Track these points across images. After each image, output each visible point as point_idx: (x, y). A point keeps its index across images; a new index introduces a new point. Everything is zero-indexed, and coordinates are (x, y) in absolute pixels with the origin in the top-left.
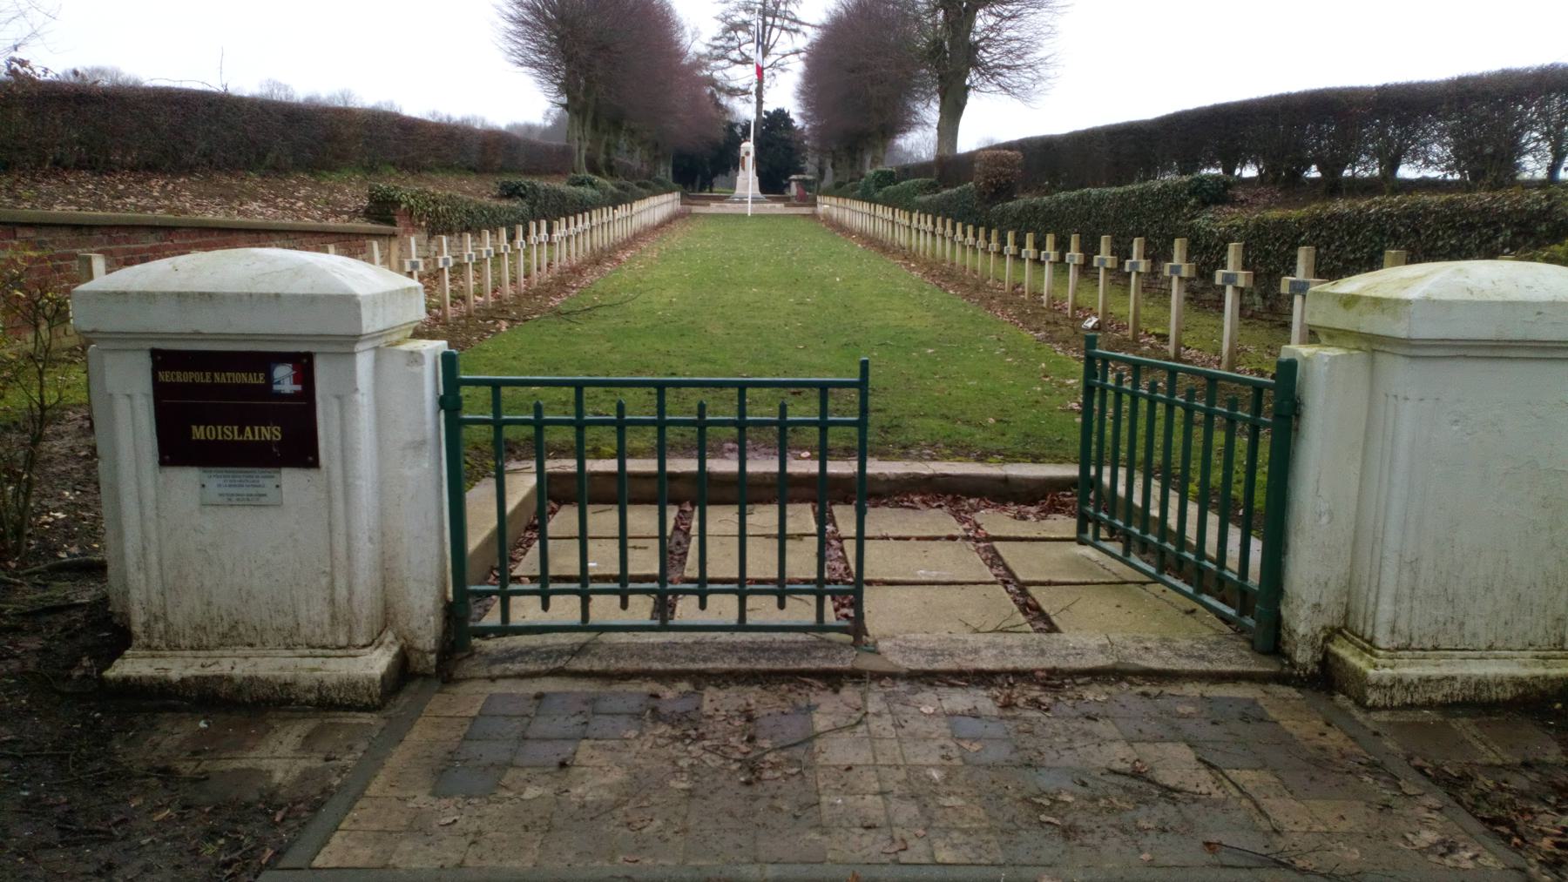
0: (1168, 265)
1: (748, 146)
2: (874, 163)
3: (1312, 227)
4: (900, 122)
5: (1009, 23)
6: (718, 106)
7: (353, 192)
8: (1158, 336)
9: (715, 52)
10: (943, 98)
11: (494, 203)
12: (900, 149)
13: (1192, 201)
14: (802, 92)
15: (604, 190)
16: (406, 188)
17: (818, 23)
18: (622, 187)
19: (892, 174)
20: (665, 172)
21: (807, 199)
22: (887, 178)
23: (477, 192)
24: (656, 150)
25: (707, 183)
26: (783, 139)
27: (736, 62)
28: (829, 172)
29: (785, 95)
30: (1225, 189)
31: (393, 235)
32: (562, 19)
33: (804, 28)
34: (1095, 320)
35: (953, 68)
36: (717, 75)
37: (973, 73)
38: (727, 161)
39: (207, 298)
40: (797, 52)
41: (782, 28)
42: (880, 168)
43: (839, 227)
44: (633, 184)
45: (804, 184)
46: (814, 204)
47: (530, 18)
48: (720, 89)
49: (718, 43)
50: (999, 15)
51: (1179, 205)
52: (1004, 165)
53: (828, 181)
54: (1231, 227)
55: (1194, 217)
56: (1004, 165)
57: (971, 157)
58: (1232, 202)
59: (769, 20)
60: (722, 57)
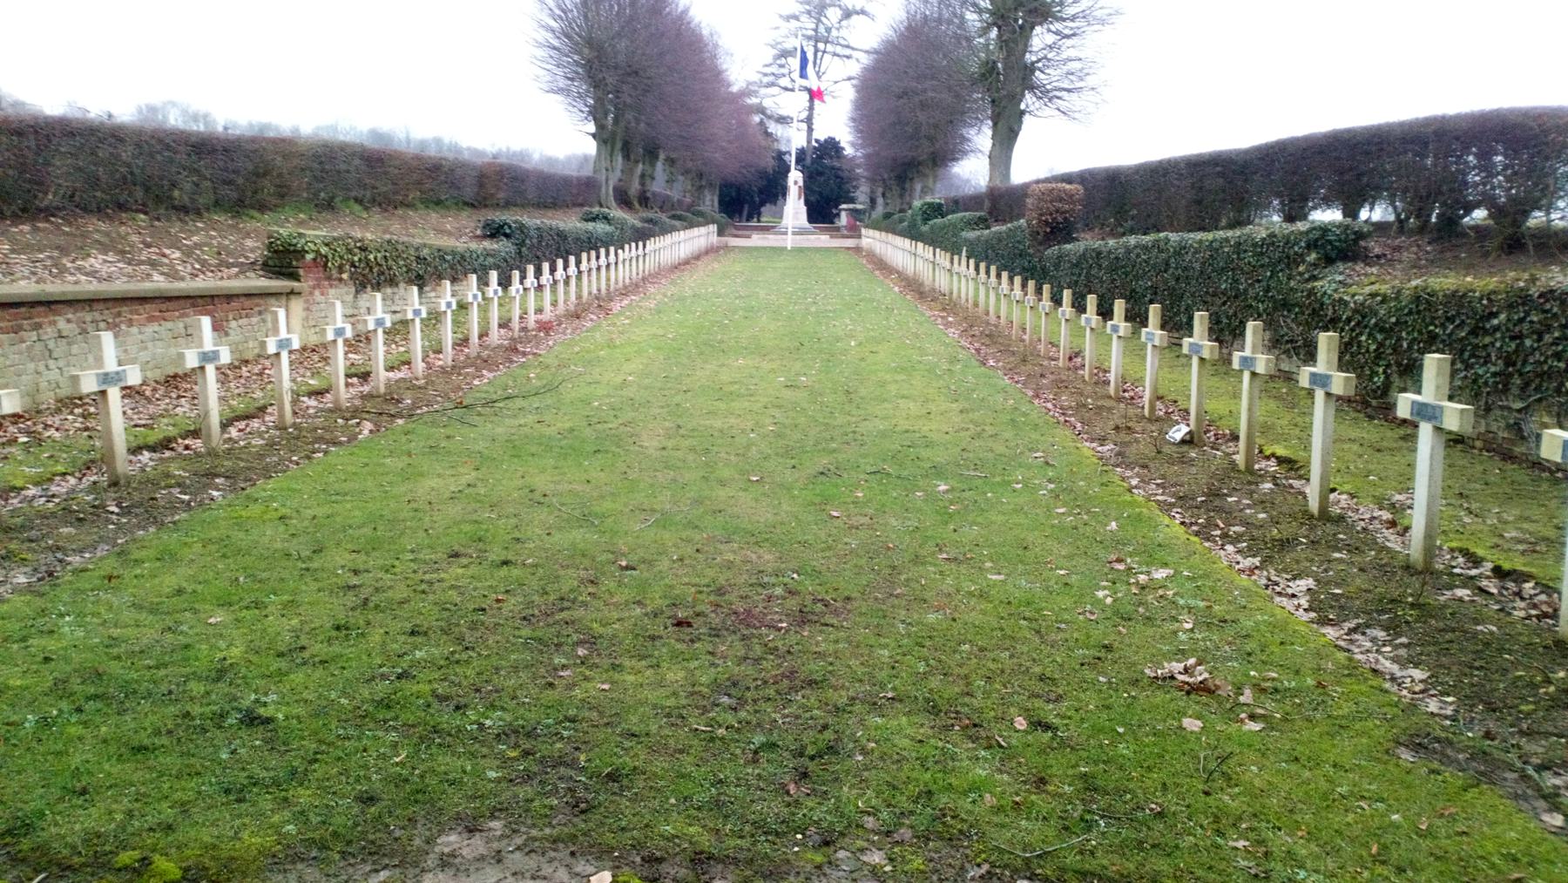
0: (1307, 370)
1: (795, 177)
2: (924, 192)
3: (1511, 306)
4: (943, 154)
5: (1068, 42)
6: (768, 135)
7: (252, 237)
8: (1281, 461)
9: (766, 80)
10: (995, 125)
11: (474, 246)
12: (958, 176)
13: (1313, 257)
14: (853, 120)
15: (622, 226)
16: (315, 234)
17: (867, 48)
18: (650, 221)
19: (940, 205)
20: (710, 202)
21: (854, 232)
22: (936, 210)
23: (450, 232)
24: (700, 179)
25: (755, 213)
26: (833, 168)
27: (786, 89)
28: (880, 201)
29: (836, 123)
30: (1356, 241)
31: (292, 293)
32: (590, 42)
33: (855, 54)
34: (1184, 429)
35: (1006, 89)
36: (767, 103)
37: (1028, 96)
38: (773, 190)
39: (1431, 469)
40: (849, 79)
41: (835, 54)
42: (929, 199)
43: (882, 265)
44: (664, 217)
45: (855, 214)
46: (859, 237)
47: (556, 43)
48: (770, 117)
49: (768, 70)
50: (1057, 33)
51: (1292, 261)
52: (1061, 200)
53: (880, 209)
54: (1373, 295)
55: (1314, 278)
56: (1061, 200)
57: (1022, 192)
58: (1367, 259)
59: (821, 46)
60: (772, 84)
